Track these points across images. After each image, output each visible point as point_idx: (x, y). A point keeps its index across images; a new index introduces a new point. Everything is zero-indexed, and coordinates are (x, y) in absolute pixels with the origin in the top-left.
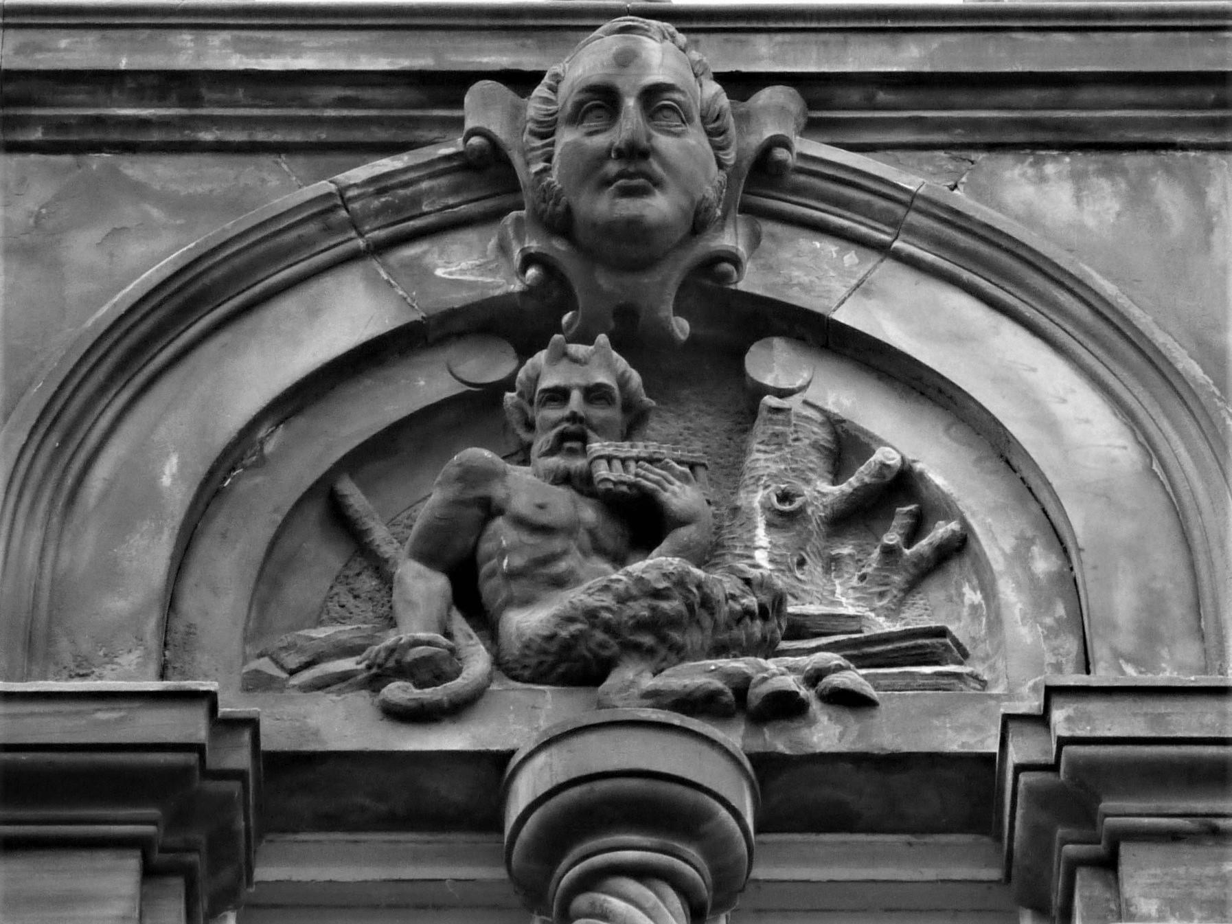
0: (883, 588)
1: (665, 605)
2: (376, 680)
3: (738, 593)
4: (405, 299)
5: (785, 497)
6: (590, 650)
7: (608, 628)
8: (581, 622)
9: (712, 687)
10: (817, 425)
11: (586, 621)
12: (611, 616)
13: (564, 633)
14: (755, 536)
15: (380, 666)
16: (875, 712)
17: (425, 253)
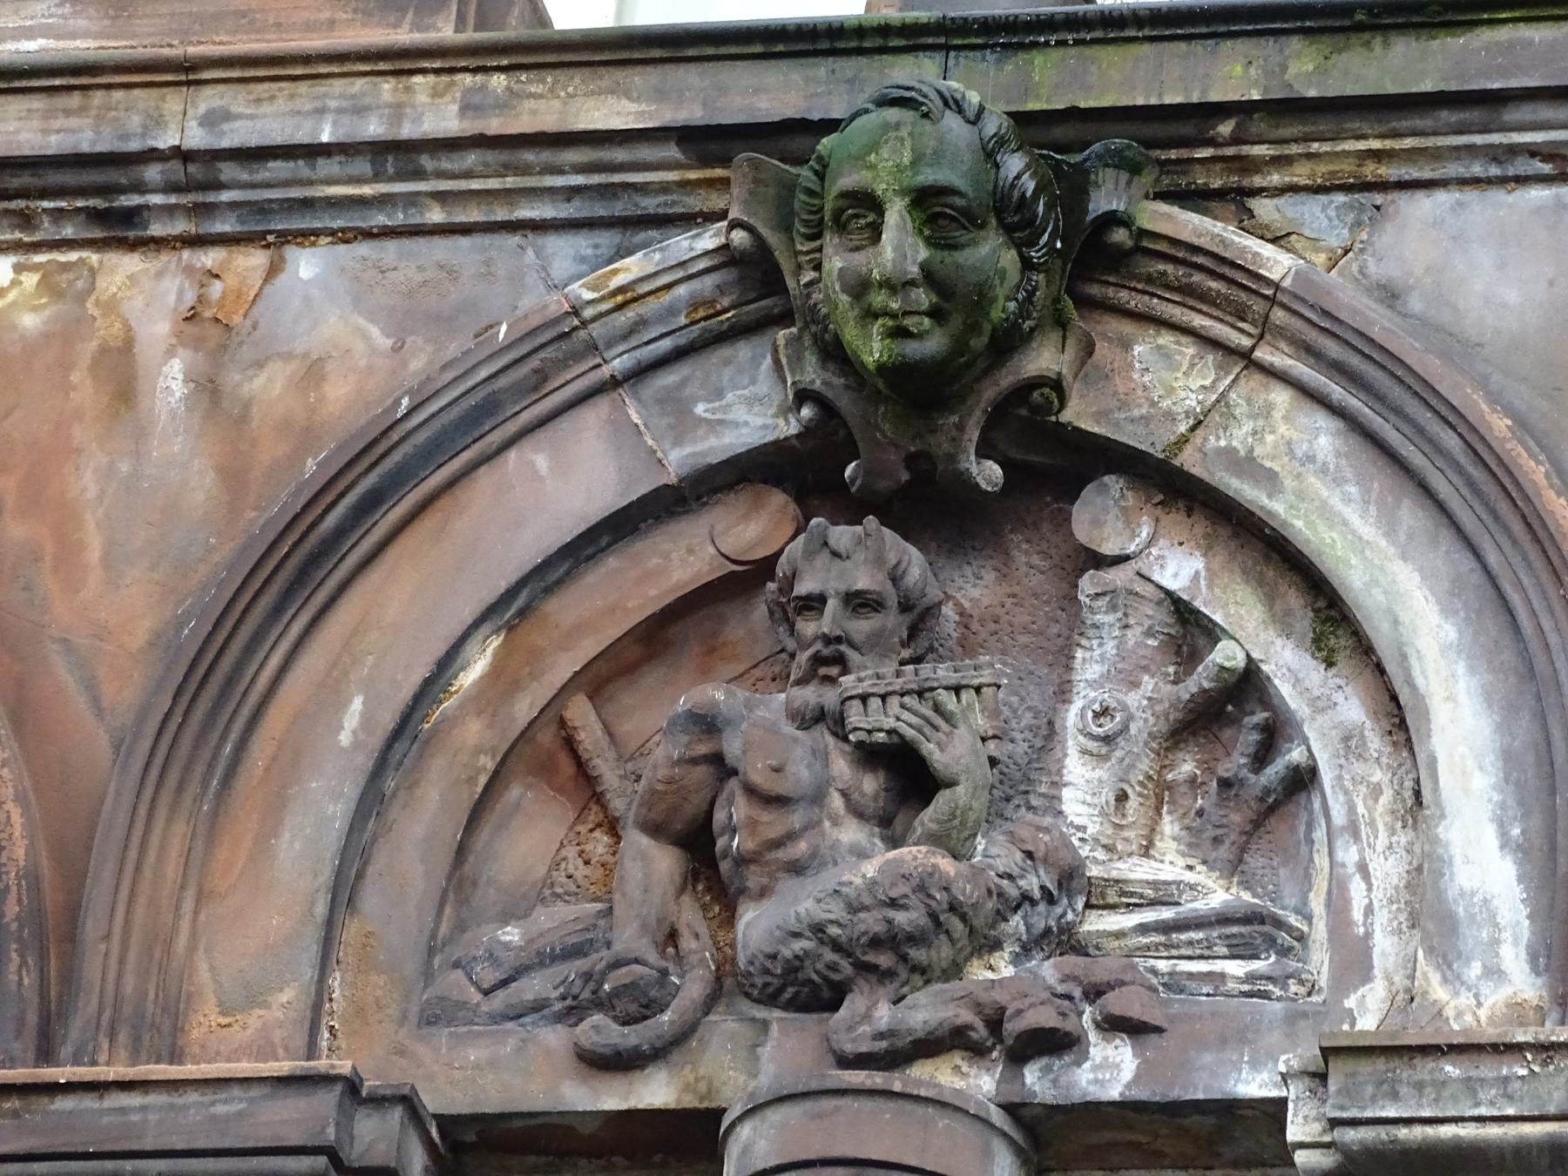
0: (1219, 832)
1: (900, 917)
2: (573, 1012)
3: (1016, 871)
4: (655, 452)
5: (1105, 712)
6: (817, 972)
7: (836, 946)
8: (808, 939)
9: (959, 1022)
10: (1151, 605)
12: (840, 932)
13: (787, 953)
14: (1063, 767)
15: (575, 998)
16: (1163, 1035)
17: (684, 382)
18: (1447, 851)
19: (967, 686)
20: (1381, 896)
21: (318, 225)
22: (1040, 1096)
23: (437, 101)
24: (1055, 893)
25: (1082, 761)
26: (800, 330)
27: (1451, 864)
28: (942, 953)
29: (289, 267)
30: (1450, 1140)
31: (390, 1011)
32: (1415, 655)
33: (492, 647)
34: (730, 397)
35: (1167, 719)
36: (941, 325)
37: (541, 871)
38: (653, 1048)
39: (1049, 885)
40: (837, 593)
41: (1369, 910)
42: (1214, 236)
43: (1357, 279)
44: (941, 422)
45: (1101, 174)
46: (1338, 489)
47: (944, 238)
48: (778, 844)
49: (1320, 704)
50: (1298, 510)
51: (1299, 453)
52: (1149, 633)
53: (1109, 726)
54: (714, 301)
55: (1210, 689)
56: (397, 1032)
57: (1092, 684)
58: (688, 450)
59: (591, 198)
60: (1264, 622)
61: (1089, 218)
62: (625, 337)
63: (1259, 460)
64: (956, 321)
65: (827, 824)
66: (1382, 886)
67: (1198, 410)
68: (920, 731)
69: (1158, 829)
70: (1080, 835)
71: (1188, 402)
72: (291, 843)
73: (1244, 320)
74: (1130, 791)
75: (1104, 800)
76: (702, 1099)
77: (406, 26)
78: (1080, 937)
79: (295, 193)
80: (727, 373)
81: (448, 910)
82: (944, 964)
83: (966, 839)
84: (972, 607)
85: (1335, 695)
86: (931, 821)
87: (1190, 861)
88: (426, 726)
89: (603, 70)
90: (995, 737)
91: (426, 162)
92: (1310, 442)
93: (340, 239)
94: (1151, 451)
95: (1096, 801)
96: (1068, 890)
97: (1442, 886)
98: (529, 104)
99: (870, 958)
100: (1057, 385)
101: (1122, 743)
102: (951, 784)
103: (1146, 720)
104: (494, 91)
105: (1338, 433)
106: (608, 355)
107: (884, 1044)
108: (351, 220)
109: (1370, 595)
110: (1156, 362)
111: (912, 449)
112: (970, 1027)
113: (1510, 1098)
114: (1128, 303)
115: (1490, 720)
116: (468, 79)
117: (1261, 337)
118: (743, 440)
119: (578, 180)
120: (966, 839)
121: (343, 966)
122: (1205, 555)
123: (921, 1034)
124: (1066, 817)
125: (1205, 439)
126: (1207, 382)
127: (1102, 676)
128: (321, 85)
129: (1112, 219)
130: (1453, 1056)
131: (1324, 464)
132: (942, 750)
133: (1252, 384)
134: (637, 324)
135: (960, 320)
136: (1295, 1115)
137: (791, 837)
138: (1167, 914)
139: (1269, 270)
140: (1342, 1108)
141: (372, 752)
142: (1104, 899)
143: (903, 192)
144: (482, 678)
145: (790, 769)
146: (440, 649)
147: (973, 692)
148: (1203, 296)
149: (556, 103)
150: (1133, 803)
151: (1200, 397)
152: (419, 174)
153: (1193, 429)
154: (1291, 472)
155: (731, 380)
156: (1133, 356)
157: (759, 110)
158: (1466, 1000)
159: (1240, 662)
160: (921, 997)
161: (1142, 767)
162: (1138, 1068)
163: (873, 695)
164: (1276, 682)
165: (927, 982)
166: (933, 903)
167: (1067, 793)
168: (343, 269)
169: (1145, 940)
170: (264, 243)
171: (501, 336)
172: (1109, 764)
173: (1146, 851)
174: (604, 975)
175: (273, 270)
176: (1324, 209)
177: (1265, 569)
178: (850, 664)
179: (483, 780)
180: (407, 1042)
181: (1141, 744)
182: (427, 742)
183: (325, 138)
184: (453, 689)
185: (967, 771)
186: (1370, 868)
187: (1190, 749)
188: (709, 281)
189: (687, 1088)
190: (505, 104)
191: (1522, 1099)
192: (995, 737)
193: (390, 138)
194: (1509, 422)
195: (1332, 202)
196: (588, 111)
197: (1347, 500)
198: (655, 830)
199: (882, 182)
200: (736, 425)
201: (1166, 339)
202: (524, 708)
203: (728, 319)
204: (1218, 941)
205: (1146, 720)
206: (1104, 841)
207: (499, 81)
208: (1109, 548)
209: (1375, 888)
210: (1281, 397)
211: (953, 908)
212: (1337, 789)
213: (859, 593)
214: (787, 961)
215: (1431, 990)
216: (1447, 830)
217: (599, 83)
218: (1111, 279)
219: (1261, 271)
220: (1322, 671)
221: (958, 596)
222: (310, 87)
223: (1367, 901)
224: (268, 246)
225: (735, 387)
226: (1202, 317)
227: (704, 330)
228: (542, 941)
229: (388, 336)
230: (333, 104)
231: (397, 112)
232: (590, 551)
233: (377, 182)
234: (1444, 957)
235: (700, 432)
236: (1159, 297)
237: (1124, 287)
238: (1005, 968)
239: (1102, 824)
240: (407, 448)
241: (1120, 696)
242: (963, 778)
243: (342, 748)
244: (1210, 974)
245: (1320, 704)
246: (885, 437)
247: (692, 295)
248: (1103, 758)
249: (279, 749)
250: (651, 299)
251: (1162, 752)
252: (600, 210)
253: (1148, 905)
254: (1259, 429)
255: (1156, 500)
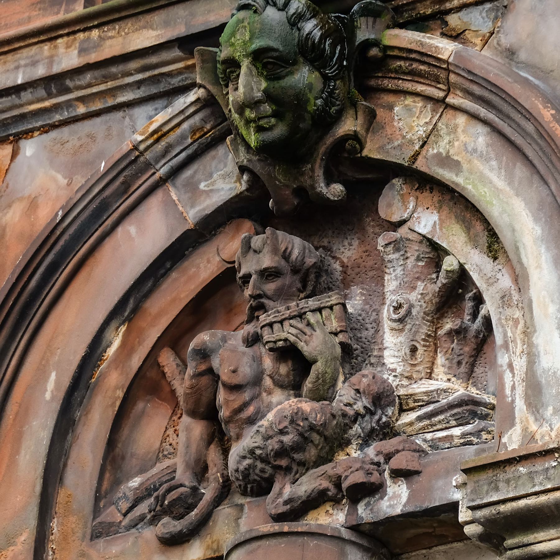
2: (154, 520)
3: (352, 401)
6: (257, 475)
7: (264, 460)
9: (321, 488)
11: (251, 457)
12: (261, 452)
13: (241, 468)
15: (154, 510)
16: (420, 474)
17: (195, 172)
18: (537, 349)
19: (324, 308)
20: (519, 379)
21: (30, 126)
22: (365, 519)
23: (69, 50)
24: (372, 409)
25: (392, 334)
26: (235, 136)
27: (539, 356)
28: (312, 453)
29: (21, 152)
30: (524, 507)
31: (78, 534)
32: (522, 246)
33: (122, 332)
34: (215, 176)
35: (432, 303)
36: (281, 121)
37: (157, 444)
38: (189, 530)
39: (369, 406)
40: (256, 272)
41: (513, 388)
42: (417, 42)
43: (496, 48)
44: (304, 169)
45: (359, 22)
46: (488, 164)
47: (273, 75)
48: (240, 409)
49: (491, 281)
50: (469, 180)
51: (470, 149)
52: (418, 259)
53: (402, 311)
54: (202, 128)
55: (446, 283)
56: (81, 545)
57: (393, 292)
58: (197, 209)
59: (149, 85)
60: (466, 242)
61: (357, 44)
62: (163, 156)
63: (452, 157)
64: (289, 116)
65: (264, 394)
66: (519, 373)
67: (424, 136)
68: (297, 337)
69: (436, 362)
70: (394, 374)
71: (419, 132)
72: (25, 456)
73: (440, 83)
74: (418, 345)
75: (403, 353)
76: (215, 552)
77: (62, 12)
78: (396, 428)
79: (16, 112)
80: (214, 164)
81: (107, 475)
82: (313, 459)
83: (328, 389)
84: (348, 262)
85: (498, 274)
86: (309, 383)
87: (449, 376)
88: (93, 380)
89: (140, 17)
90: (341, 331)
91: (69, 83)
92: (475, 142)
93: (42, 131)
94: (403, 163)
95: (400, 354)
96: (380, 406)
97: (535, 369)
98: (108, 43)
99: (277, 463)
100: (355, 136)
101: (409, 321)
102: (315, 361)
103: (421, 306)
104: (93, 39)
105: (488, 133)
106: (158, 167)
107: (288, 507)
108: (45, 120)
109: (502, 218)
110: (404, 114)
111: (295, 186)
112: (327, 490)
113: (548, 479)
114: (388, 85)
115: (556, 274)
116: (81, 36)
117: (449, 90)
118: (222, 198)
119: (139, 77)
120: (328, 389)
121: (58, 515)
122: (439, 212)
123: (304, 498)
124: (386, 366)
125: (428, 151)
126: (427, 120)
127: (397, 287)
128: (18, 54)
129: (368, 44)
130: (523, 462)
131: (481, 152)
132: (307, 345)
133: (448, 116)
134: (167, 147)
135: (291, 115)
136: (462, 508)
137: (245, 405)
138: (430, 408)
139: (442, 54)
140: (473, 500)
141: (59, 401)
142: (408, 405)
143: (247, 56)
144: (118, 349)
145: (241, 370)
146: (88, 339)
147: (328, 310)
148: (420, 74)
149: (120, 39)
150: (421, 350)
151: (425, 129)
152: (68, 90)
153: (422, 146)
154: (466, 160)
155: (216, 167)
156: (394, 113)
157: (210, 21)
158: (546, 428)
159: (455, 266)
160: (304, 479)
161: (423, 331)
162: (409, 494)
163: (275, 322)
164: (471, 273)
165: (307, 470)
166: (300, 428)
167: (386, 353)
168: (45, 147)
169: (421, 424)
170: (9, 141)
171: (102, 168)
172: (405, 333)
173: (430, 376)
174: (164, 496)
175: (14, 154)
176: (481, 14)
177: (466, 213)
178: (267, 307)
179: (118, 403)
180: (85, 549)
181: (420, 319)
182: (94, 387)
183: (19, 82)
184: (105, 358)
185: (321, 353)
186: (514, 365)
187: (449, 316)
188: (197, 118)
189: (208, 548)
190: (97, 46)
191: (554, 478)
192: (341, 331)
193: (48, 75)
194: (553, 112)
195: (484, 9)
196: (134, 40)
197: (492, 169)
198: (193, 414)
199: (237, 52)
200: (218, 190)
201: (409, 101)
202: (136, 361)
203: (210, 136)
204: (450, 418)
205: (421, 306)
206: (406, 374)
207: (95, 33)
208: (395, 218)
209: (516, 375)
210: (461, 120)
211: (312, 428)
212: (499, 325)
213: (266, 270)
214: (243, 472)
215: (530, 427)
216: (537, 338)
217: (139, 24)
218: (380, 75)
219: (439, 56)
220: (492, 263)
221: (342, 257)
222: (12, 56)
223: (512, 383)
224: (11, 143)
225: (218, 171)
226: (421, 85)
227: (200, 144)
228: (149, 482)
229: (65, 178)
230: (22, 62)
231: (51, 59)
232: (162, 271)
233: (51, 98)
234: (536, 407)
235: (202, 198)
236: (403, 80)
237: (386, 77)
238: (354, 452)
239: (404, 365)
240: (66, 237)
241: (405, 296)
242: (319, 358)
243: (47, 401)
244: (447, 437)
245: (491, 281)
246: (281, 183)
247: (191, 127)
248: (401, 330)
249: (20, 407)
250: (171, 133)
251: (435, 320)
252: (154, 90)
253: (426, 405)
254: (451, 140)
255: (416, 187)
